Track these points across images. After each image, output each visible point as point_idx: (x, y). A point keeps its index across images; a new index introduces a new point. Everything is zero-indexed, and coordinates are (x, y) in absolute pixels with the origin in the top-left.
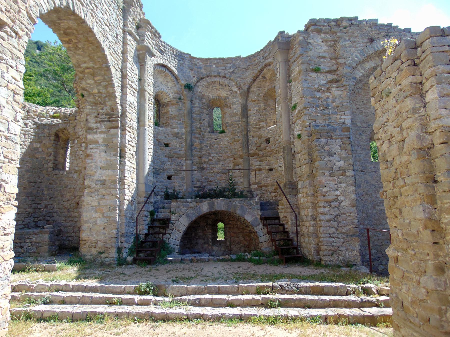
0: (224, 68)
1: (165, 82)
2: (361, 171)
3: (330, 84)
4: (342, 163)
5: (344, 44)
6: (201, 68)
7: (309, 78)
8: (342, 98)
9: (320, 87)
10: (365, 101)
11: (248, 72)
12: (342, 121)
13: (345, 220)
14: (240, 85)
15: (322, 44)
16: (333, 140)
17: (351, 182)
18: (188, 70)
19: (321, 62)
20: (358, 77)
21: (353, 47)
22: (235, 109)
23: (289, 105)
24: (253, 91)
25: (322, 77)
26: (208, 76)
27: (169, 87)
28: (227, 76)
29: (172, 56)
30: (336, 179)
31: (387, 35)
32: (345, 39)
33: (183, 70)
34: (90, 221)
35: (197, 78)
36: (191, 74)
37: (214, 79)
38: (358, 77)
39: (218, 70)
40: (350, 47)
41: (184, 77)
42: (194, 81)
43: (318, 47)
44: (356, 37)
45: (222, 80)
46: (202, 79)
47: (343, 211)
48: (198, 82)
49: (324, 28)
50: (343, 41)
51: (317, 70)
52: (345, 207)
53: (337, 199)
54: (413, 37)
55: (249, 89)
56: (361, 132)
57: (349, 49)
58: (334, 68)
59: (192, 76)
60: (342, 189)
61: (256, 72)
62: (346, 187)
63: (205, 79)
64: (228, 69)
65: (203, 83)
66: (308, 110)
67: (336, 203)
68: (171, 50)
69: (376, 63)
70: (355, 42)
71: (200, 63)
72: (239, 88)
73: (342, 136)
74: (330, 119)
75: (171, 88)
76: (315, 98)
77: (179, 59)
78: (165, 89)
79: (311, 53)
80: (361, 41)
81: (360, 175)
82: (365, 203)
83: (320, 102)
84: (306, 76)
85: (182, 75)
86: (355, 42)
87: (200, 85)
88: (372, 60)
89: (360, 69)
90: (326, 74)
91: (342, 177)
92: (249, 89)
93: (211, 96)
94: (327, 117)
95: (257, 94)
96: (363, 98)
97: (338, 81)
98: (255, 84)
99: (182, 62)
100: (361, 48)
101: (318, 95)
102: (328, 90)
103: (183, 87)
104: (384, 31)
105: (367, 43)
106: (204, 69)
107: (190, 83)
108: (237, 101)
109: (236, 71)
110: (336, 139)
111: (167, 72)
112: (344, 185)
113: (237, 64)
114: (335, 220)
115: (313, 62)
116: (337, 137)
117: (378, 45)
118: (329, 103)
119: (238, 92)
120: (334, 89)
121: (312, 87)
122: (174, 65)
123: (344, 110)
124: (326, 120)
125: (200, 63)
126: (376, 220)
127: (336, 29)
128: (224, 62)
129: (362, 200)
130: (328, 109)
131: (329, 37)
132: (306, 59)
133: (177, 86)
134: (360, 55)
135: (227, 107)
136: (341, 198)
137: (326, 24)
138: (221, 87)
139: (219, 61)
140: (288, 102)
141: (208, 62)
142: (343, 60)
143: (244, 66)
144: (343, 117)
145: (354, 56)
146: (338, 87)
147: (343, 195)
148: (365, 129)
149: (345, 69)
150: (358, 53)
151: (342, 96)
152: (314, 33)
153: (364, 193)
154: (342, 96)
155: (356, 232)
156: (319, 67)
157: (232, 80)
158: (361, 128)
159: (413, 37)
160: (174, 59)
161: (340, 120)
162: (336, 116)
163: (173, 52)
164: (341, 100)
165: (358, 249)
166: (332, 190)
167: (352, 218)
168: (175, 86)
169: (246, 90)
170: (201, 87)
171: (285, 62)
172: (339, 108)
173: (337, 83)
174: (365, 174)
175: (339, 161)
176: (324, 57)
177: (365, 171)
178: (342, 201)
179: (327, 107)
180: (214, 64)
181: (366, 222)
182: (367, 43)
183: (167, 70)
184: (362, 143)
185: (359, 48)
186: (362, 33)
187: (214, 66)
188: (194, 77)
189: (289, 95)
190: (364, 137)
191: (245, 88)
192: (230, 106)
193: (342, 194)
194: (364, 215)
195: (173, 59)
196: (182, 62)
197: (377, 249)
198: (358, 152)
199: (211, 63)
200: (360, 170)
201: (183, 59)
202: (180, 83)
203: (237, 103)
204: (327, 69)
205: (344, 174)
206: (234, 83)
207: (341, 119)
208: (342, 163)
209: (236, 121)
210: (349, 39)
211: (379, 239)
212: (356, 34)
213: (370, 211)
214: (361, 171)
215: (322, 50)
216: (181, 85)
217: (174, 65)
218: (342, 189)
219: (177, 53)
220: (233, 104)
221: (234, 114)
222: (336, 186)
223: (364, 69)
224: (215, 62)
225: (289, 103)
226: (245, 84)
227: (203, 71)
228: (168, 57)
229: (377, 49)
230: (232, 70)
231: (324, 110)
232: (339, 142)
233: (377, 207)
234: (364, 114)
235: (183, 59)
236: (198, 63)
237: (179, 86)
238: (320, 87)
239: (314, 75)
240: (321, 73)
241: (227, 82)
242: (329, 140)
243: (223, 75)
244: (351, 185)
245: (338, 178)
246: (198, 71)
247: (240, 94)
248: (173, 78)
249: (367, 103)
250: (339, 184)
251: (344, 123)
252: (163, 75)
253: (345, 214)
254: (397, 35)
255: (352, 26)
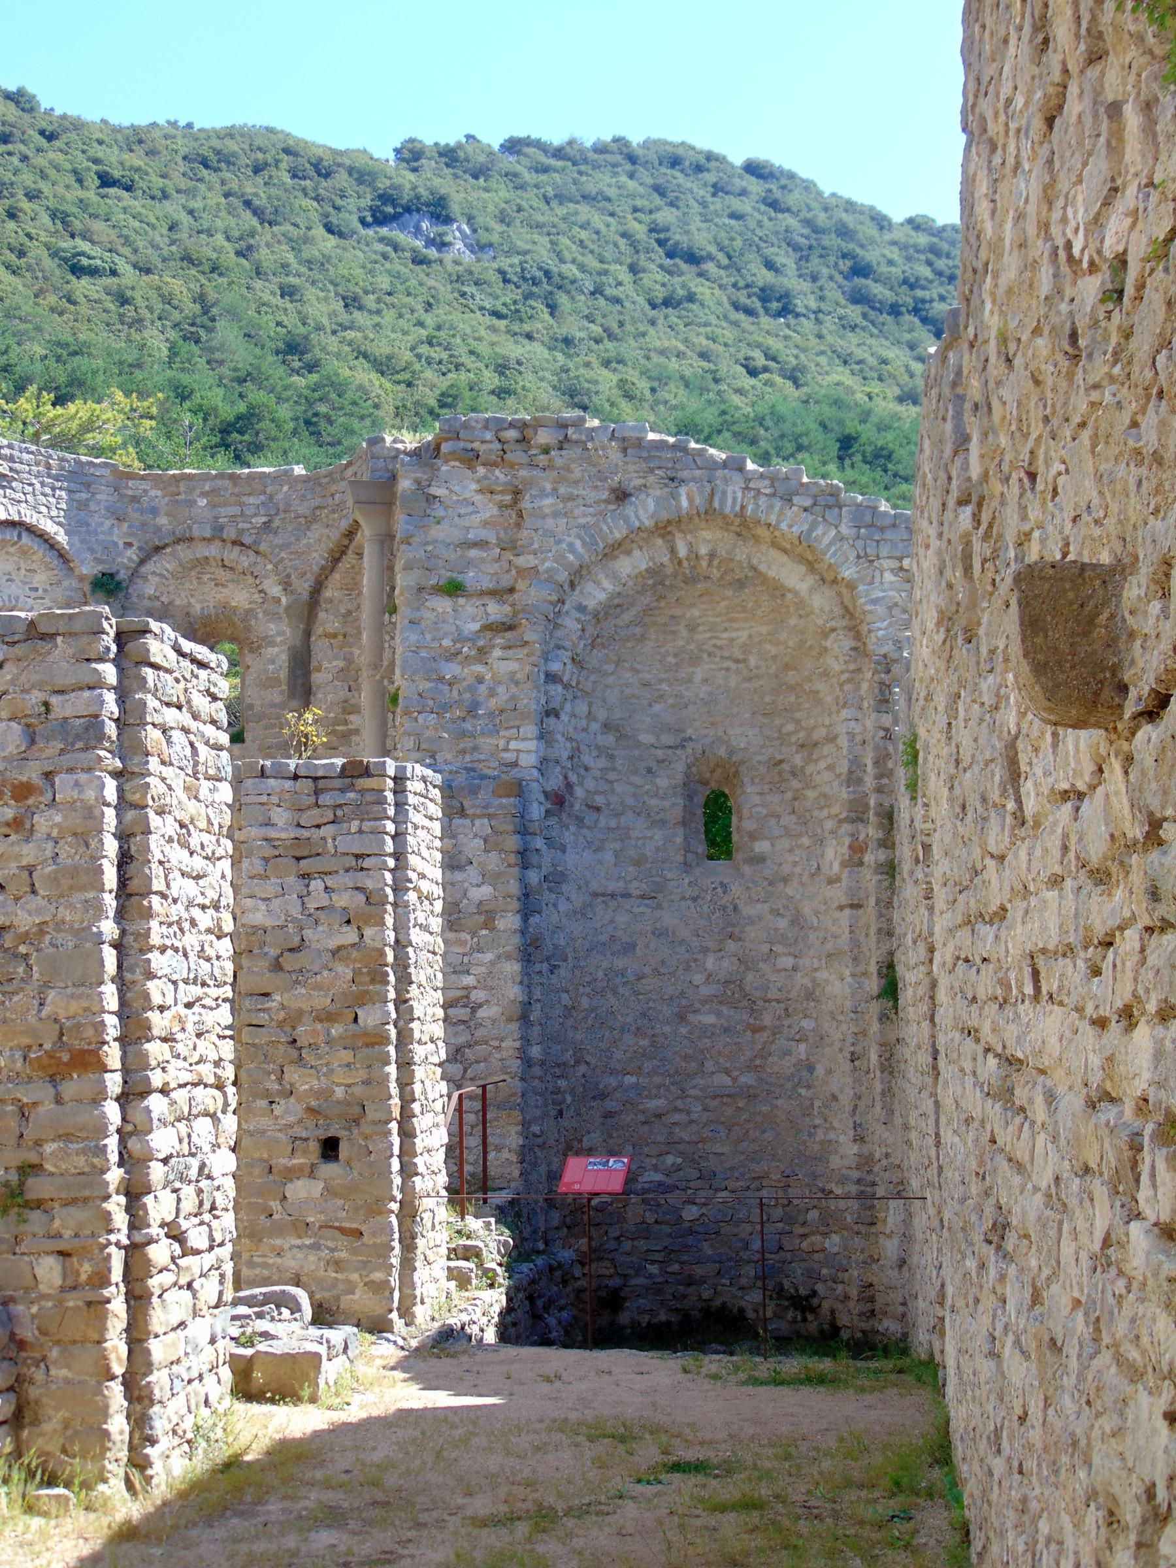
0: (236, 510)
1: (23, 571)
2: (642, 897)
3: (489, 634)
4: (486, 891)
5: (535, 505)
6: (154, 511)
7: (428, 615)
8: (517, 683)
9: (458, 646)
10: (671, 660)
11: (316, 531)
12: (509, 757)
13: (485, 1060)
14: (289, 576)
15: (478, 498)
16: (467, 822)
17: (508, 948)
18: (108, 523)
19: (470, 563)
20: (591, 604)
21: (565, 515)
22: (273, 662)
23: (384, 688)
24: (331, 601)
25: (470, 609)
26: (178, 541)
27: (36, 589)
28: (247, 540)
29: (43, 484)
30: (468, 937)
31: (672, 479)
32: (543, 490)
33: (88, 525)
34: (1155, 607)
35: (140, 549)
36: (119, 535)
37: (202, 551)
38: (591, 604)
39: (217, 518)
40: (556, 515)
41: (92, 550)
42: (130, 559)
43: (462, 511)
44: (576, 482)
45: (233, 555)
46: (158, 549)
47: (479, 1033)
48: (142, 562)
49: (485, 447)
50: (535, 497)
51: (454, 589)
52: (488, 1023)
53: (467, 997)
54: (752, 485)
55: (317, 589)
56: (653, 764)
57: (550, 523)
58: (506, 582)
59: (121, 544)
60: (483, 969)
61: (335, 534)
62: (492, 963)
63: (168, 550)
64: (248, 513)
65: (164, 564)
66: (416, 720)
67: (463, 1011)
68: (37, 464)
69: (651, 559)
70: (571, 498)
71: (153, 493)
72: (287, 585)
73: (491, 811)
74: (475, 749)
75: (45, 590)
76: (441, 679)
77: (73, 486)
78: (22, 598)
79: (437, 532)
80: (591, 495)
81: (636, 910)
82: (651, 1004)
83: (455, 694)
84: (418, 609)
85: (83, 541)
86: (571, 498)
87: (154, 573)
88: (641, 548)
89: (602, 576)
90: (486, 600)
91: (484, 932)
92: (317, 589)
93: (198, 607)
94: (467, 743)
95: (343, 611)
96: (663, 650)
97: (511, 628)
98: (336, 576)
99: (84, 496)
100: (589, 519)
101: (451, 670)
102: (482, 653)
103: (87, 588)
104: (663, 464)
105: (608, 502)
106: (167, 515)
107: (113, 571)
108: (279, 634)
109: (277, 523)
110: (474, 817)
111: (26, 539)
112: (489, 957)
113: (280, 496)
114: (456, 1060)
115: (441, 563)
116: (478, 812)
117: (641, 512)
118: (481, 699)
119: (284, 600)
120: (497, 653)
121: (436, 645)
122: (54, 513)
123: (517, 723)
124: (463, 752)
125: (153, 493)
126: (686, 1057)
127: (517, 456)
128: (237, 490)
129: (637, 993)
130: (474, 717)
131: (502, 476)
132: (420, 554)
133: (66, 583)
134: (584, 544)
135: (251, 651)
136: (478, 996)
137: (489, 436)
138: (229, 575)
139: (219, 483)
140: (383, 678)
141: (182, 489)
142: (531, 557)
143: (303, 509)
144: (513, 745)
145: (564, 546)
146: (510, 648)
147: (484, 988)
148: (670, 752)
149: (533, 591)
150: (579, 537)
151: (518, 676)
152: (453, 463)
153: (647, 970)
154: (518, 676)
155: (514, 1095)
156: (460, 578)
157: (265, 556)
158: (653, 751)
159: (752, 485)
160: (53, 489)
161: (505, 755)
162: (493, 741)
163: (49, 467)
164: (513, 689)
165: (514, 1146)
166: (454, 972)
167: (505, 1054)
168: (59, 583)
169: (306, 596)
170: (157, 579)
171: (382, 542)
172: (500, 719)
173: (508, 634)
174: (660, 906)
175: (478, 886)
176: (481, 544)
177: (660, 896)
178: (480, 1006)
179: (472, 711)
180: (203, 494)
181: (648, 1066)
182: (608, 502)
183: (25, 534)
184: (653, 802)
185: (582, 521)
186: (595, 470)
187: (202, 502)
188: (129, 545)
189: (387, 654)
190: (663, 782)
191: (303, 587)
192: (259, 647)
193: (481, 984)
194: (645, 1042)
195: (48, 490)
196: (84, 496)
197: (681, 1154)
198: (633, 834)
199: (191, 491)
200: (635, 893)
201: (88, 485)
202: (77, 572)
203: (279, 639)
204: (487, 584)
205: (489, 924)
206: (270, 567)
207: (506, 750)
208: (486, 891)
209: (273, 705)
210: (555, 490)
211: (692, 1122)
212: (577, 473)
213: (667, 1029)
214: (642, 897)
215: (476, 519)
216: (81, 579)
217: (54, 513)
218: (483, 969)
219: (62, 468)
220: (269, 641)
221: (268, 679)
222: (466, 960)
223: (614, 576)
224: (207, 488)
225: (386, 682)
226: (304, 574)
227: (163, 521)
228: (29, 489)
229: (637, 524)
230: (264, 519)
231: (464, 719)
232: (483, 826)
233: (691, 1017)
234: (671, 701)
235: (88, 485)
236: (145, 491)
237: (74, 583)
238: (458, 646)
239: (443, 604)
240: (469, 596)
241: (245, 560)
242: (457, 822)
243: (233, 536)
244: (509, 957)
245: (474, 934)
246: (144, 524)
247: (288, 608)
248: (51, 558)
249: (676, 664)
250: (476, 955)
251: (515, 764)
252: (12, 550)
253: (486, 1043)
254: (701, 480)
255: (566, 446)
